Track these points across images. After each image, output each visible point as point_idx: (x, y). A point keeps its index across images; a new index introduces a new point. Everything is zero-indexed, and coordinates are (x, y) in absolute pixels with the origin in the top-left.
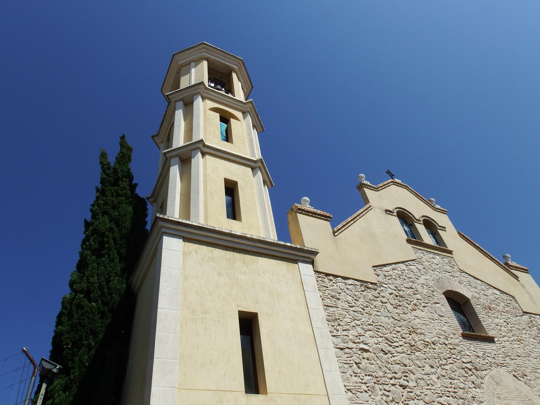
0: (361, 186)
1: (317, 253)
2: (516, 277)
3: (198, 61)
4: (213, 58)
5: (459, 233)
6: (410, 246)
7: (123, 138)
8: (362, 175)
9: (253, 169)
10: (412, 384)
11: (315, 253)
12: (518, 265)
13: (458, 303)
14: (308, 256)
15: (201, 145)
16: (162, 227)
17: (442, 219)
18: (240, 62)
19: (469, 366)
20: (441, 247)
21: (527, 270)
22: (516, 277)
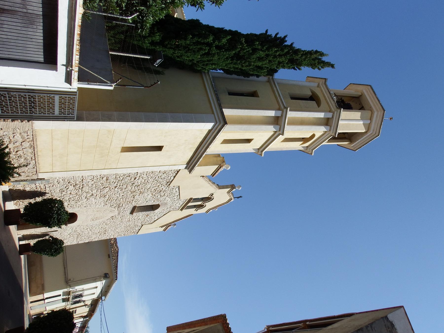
0: (233, 187)
1: (190, 173)
2: (162, 227)
3: (368, 127)
4: (365, 136)
5: (192, 215)
6: (189, 198)
7: (332, 66)
8: (240, 189)
9: (259, 149)
10: (116, 189)
11: (190, 172)
12: (219, 171)
13: (153, 208)
14: (191, 165)
15: (281, 132)
16: (220, 123)
17: (202, 211)
18: (355, 149)
19: (121, 205)
20: (185, 206)
21: (213, 176)
22: (162, 227)
